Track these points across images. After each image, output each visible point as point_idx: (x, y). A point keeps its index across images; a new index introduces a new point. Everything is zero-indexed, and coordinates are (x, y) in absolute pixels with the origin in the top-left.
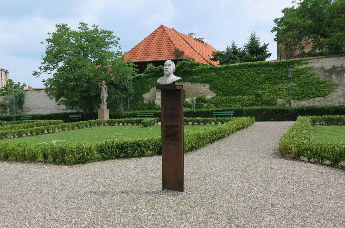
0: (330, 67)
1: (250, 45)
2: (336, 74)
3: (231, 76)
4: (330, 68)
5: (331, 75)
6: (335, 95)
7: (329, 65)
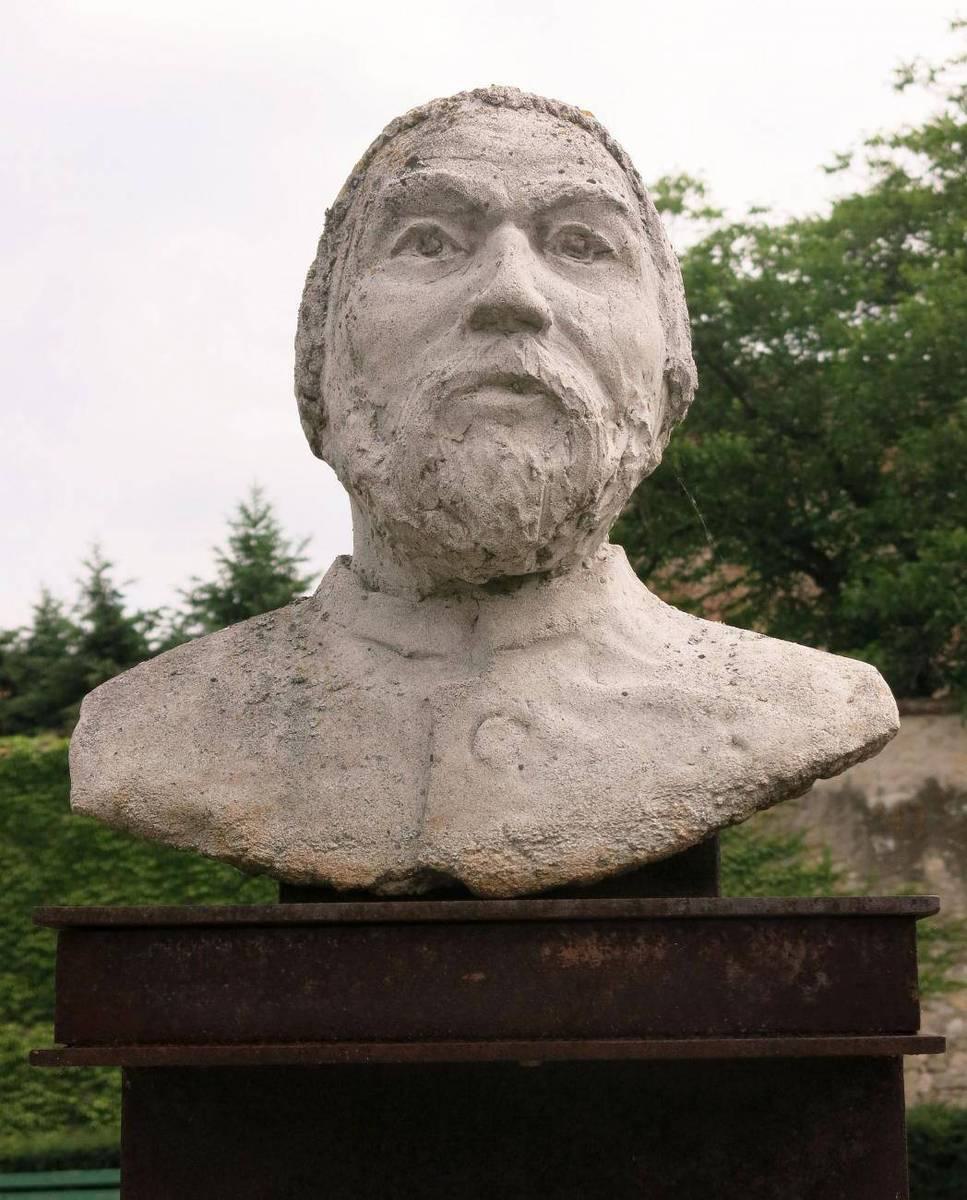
0: (902, 789)
1: (229, 593)
2: (952, 848)
3: (107, 841)
4: (905, 797)
5: (916, 854)
6: (954, 1016)
7: (894, 778)
